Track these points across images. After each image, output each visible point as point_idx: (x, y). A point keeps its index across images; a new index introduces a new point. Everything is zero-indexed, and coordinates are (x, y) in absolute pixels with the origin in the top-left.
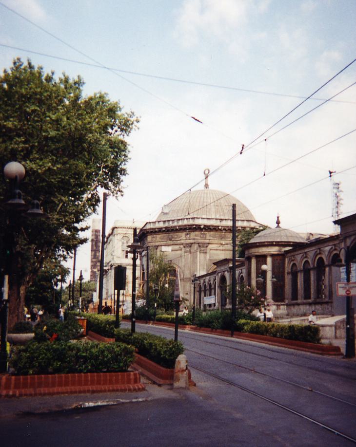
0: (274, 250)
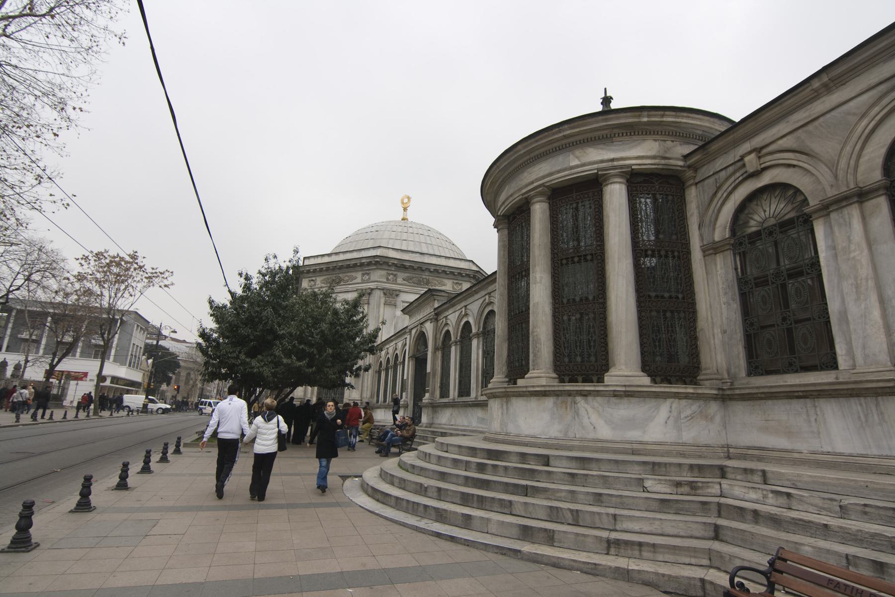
0: (640, 153)
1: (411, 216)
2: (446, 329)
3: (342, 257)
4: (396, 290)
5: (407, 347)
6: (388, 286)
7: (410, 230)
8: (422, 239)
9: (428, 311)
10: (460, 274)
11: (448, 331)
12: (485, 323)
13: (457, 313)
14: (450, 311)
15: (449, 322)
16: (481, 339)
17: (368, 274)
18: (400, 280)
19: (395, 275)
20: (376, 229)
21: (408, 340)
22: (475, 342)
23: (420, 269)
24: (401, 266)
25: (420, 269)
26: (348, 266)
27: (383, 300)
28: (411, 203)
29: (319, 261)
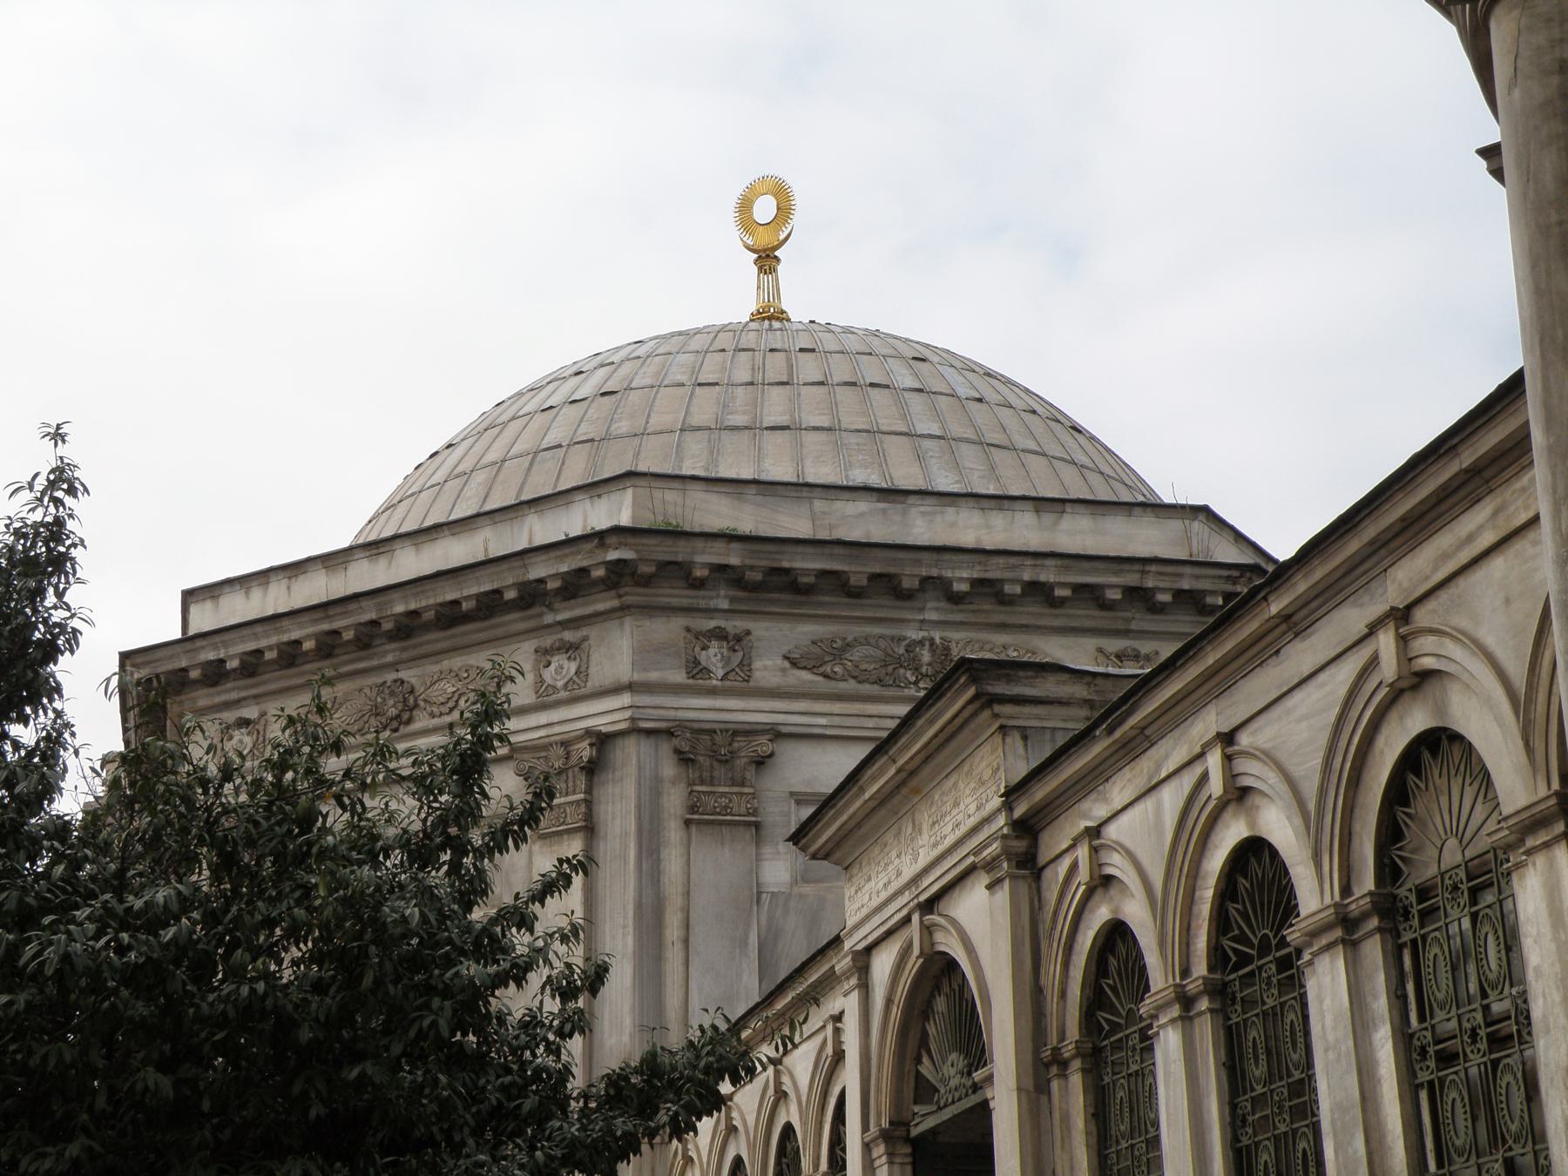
1: (800, 305)
2: (1101, 914)
3: (410, 564)
4: (750, 732)
5: (850, 1077)
6: (697, 708)
7: (809, 369)
8: (884, 411)
9: (968, 805)
10: (1139, 596)
11: (1117, 932)
12: (1391, 833)
13: (1171, 799)
14: (1119, 790)
15: (1116, 864)
16: (1373, 951)
17: (570, 649)
18: (768, 668)
19: (737, 641)
20: (611, 383)
21: (851, 1026)
22: (1327, 985)
23: (888, 586)
24: (774, 579)
25: (888, 586)
26: (451, 616)
27: (674, 800)
28: (797, 219)
29: (276, 599)
